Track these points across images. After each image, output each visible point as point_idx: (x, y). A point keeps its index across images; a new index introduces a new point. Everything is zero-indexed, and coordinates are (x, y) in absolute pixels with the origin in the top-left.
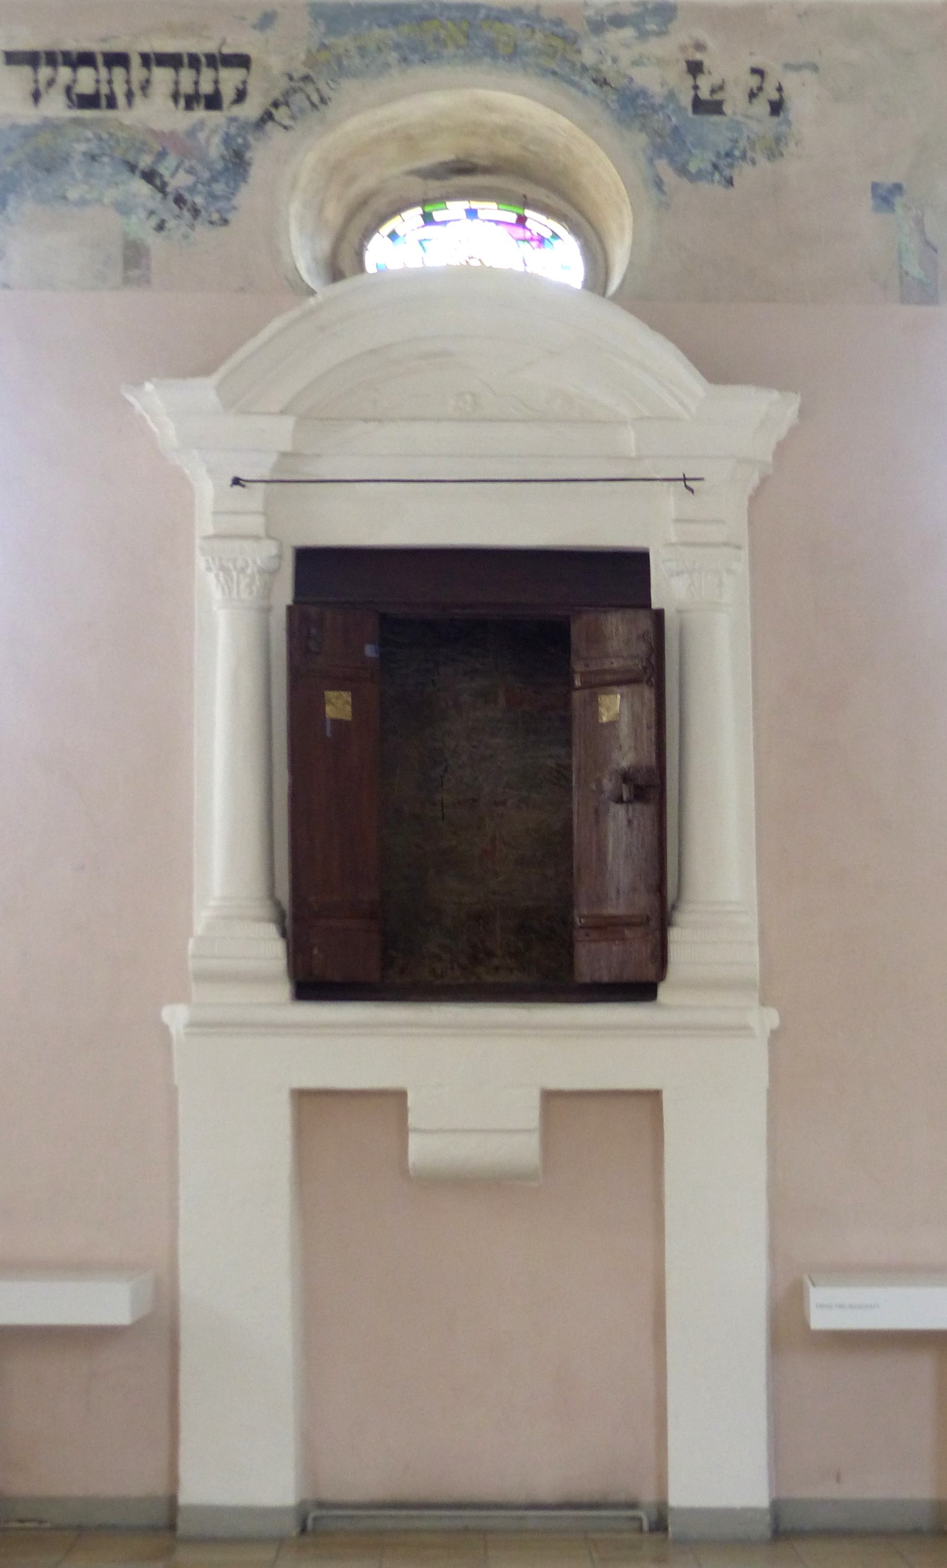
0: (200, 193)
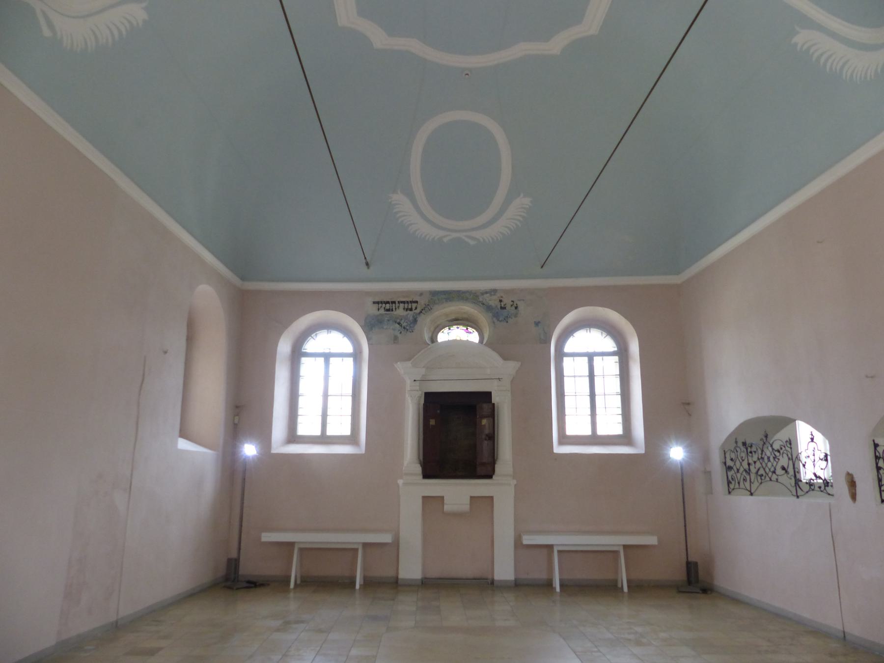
0: (409, 326)
